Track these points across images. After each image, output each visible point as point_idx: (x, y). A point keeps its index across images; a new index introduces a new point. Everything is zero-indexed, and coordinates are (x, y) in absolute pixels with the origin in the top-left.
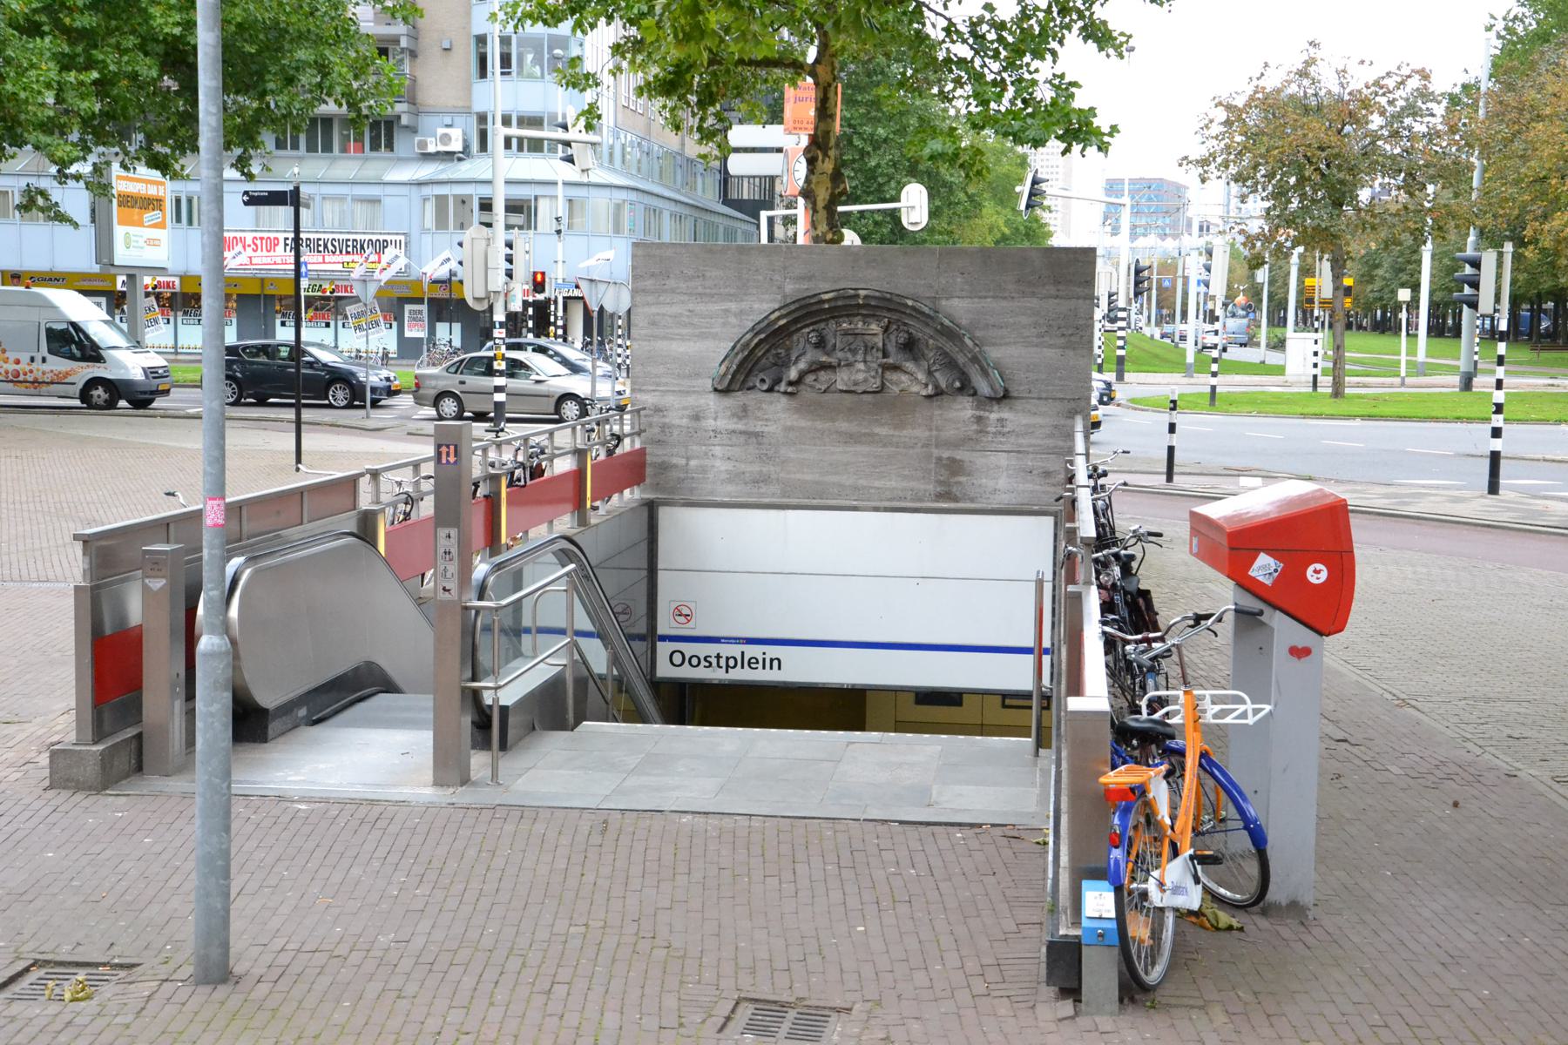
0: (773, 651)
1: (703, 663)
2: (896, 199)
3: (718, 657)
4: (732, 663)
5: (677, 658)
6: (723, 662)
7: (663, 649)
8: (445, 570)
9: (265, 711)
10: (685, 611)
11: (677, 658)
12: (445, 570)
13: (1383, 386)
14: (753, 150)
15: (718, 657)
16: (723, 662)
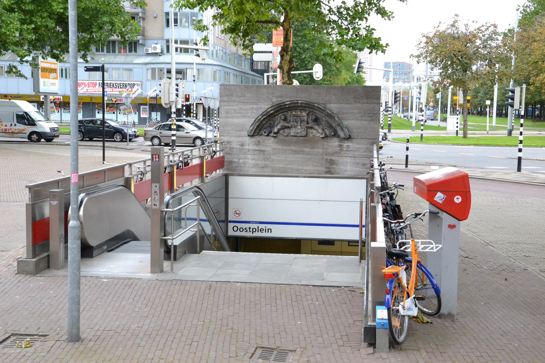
0: (269, 226)
1: (244, 230)
2: (312, 69)
3: (250, 228)
4: (254, 230)
5: (235, 229)
6: (251, 230)
7: (231, 225)
8: (155, 198)
9: (92, 247)
10: (238, 212)
11: (235, 229)
12: (155, 198)
13: (481, 134)
14: (262, 52)
15: (250, 228)
16: (251, 230)
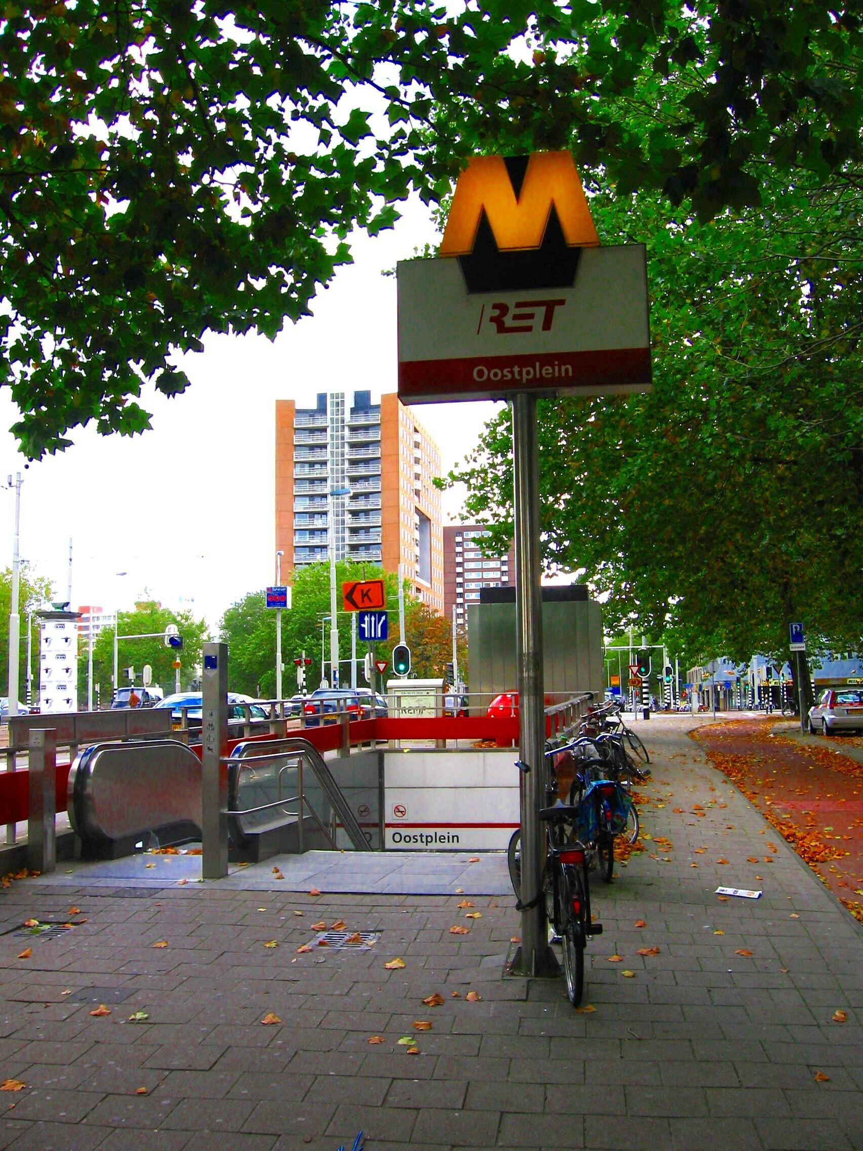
0: (453, 831)
1: (413, 840)
2: (164, 631)
3: (421, 836)
4: (429, 839)
5: (397, 838)
6: (424, 839)
7: (389, 832)
8: (209, 736)
9: (111, 841)
10: (402, 809)
11: (397, 838)
12: (209, 736)
13: (530, 785)
14: (18, 517)
15: (421, 836)
16: (424, 839)
